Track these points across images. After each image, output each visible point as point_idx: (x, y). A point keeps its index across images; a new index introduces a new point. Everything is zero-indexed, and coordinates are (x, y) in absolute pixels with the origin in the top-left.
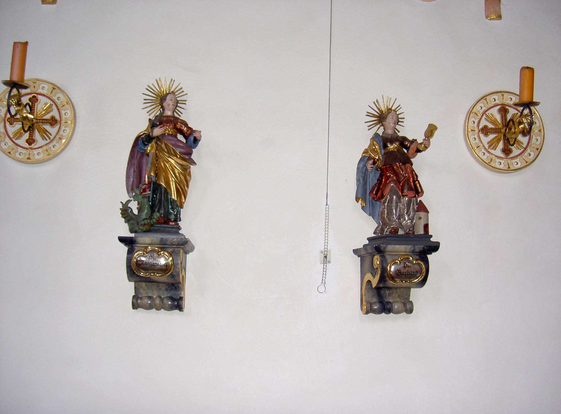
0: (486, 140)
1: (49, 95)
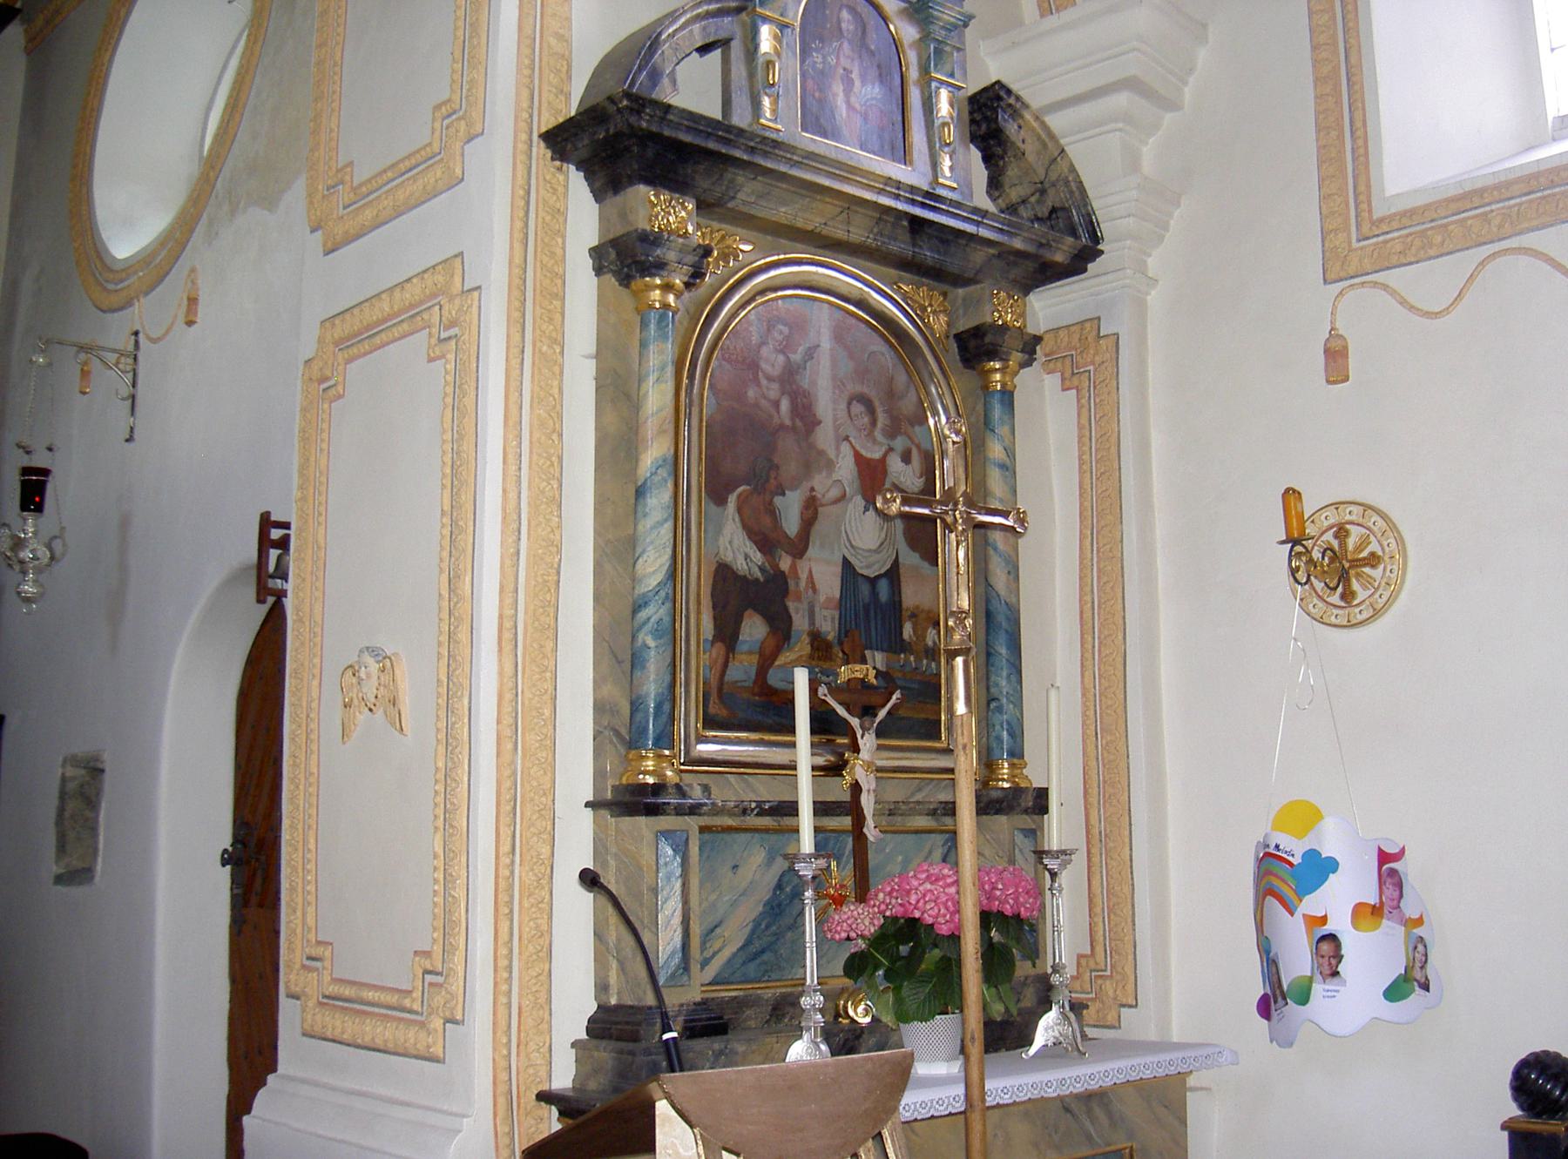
0: (1374, 547)
1: (1361, 520)
